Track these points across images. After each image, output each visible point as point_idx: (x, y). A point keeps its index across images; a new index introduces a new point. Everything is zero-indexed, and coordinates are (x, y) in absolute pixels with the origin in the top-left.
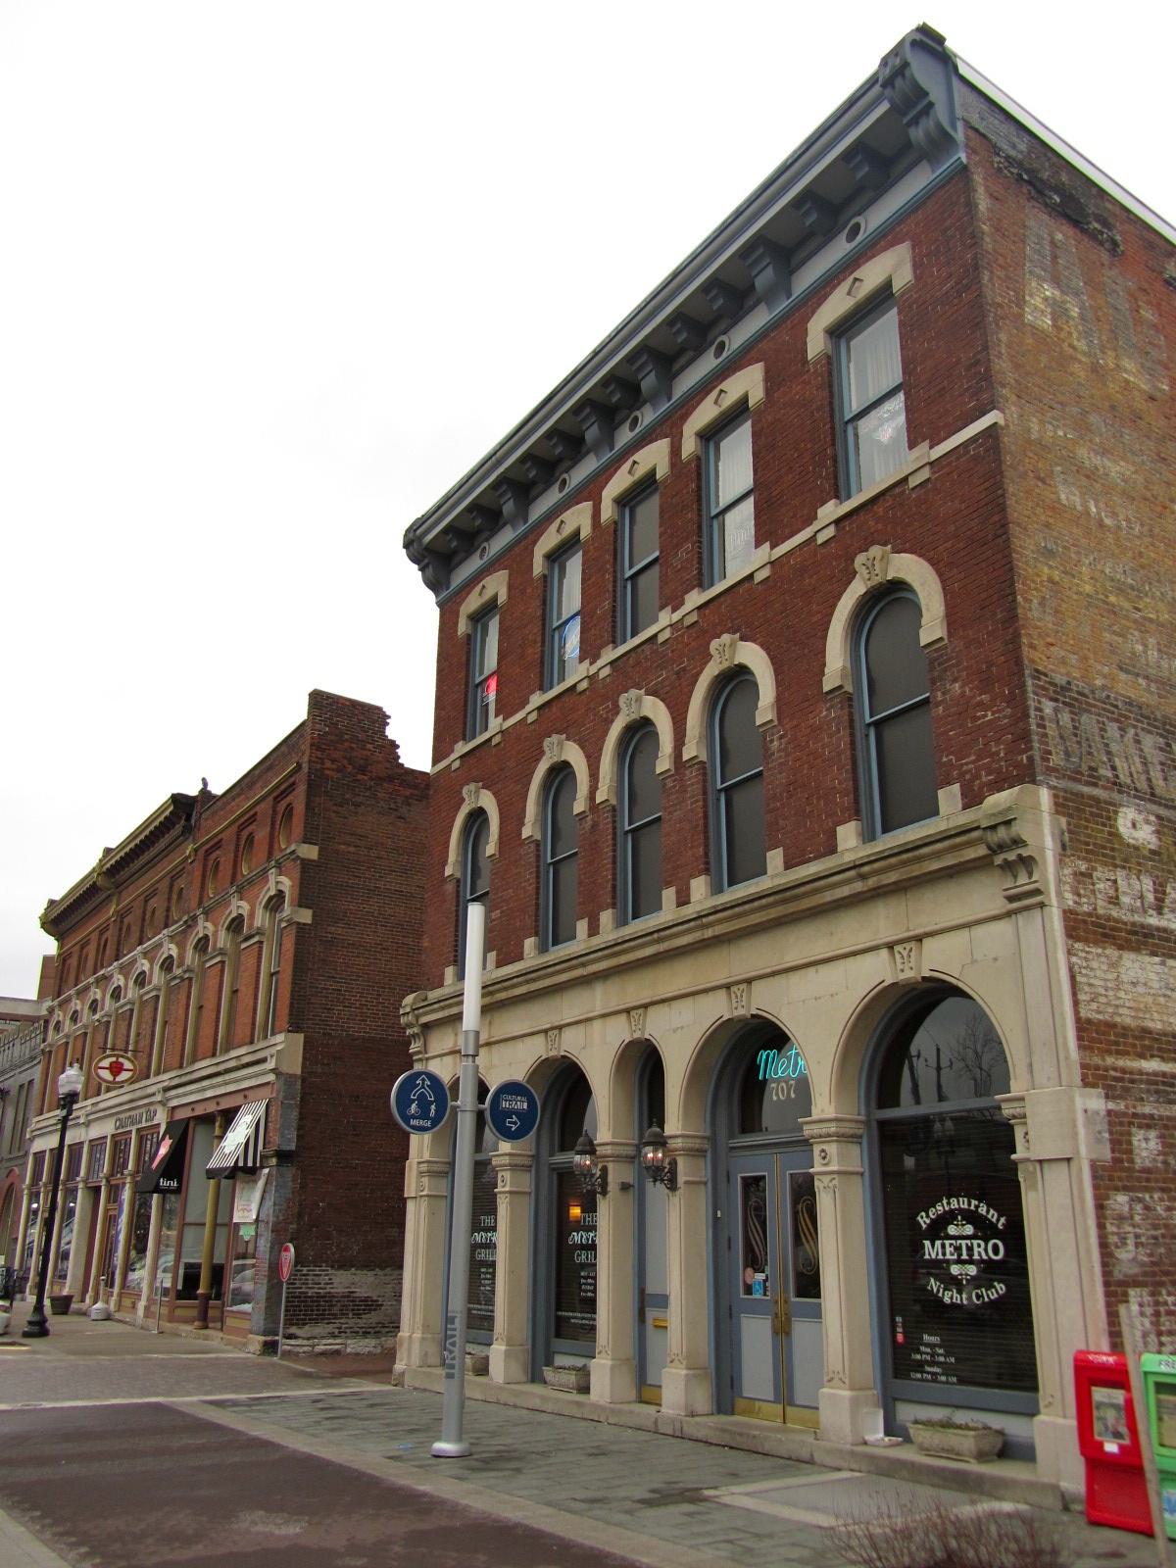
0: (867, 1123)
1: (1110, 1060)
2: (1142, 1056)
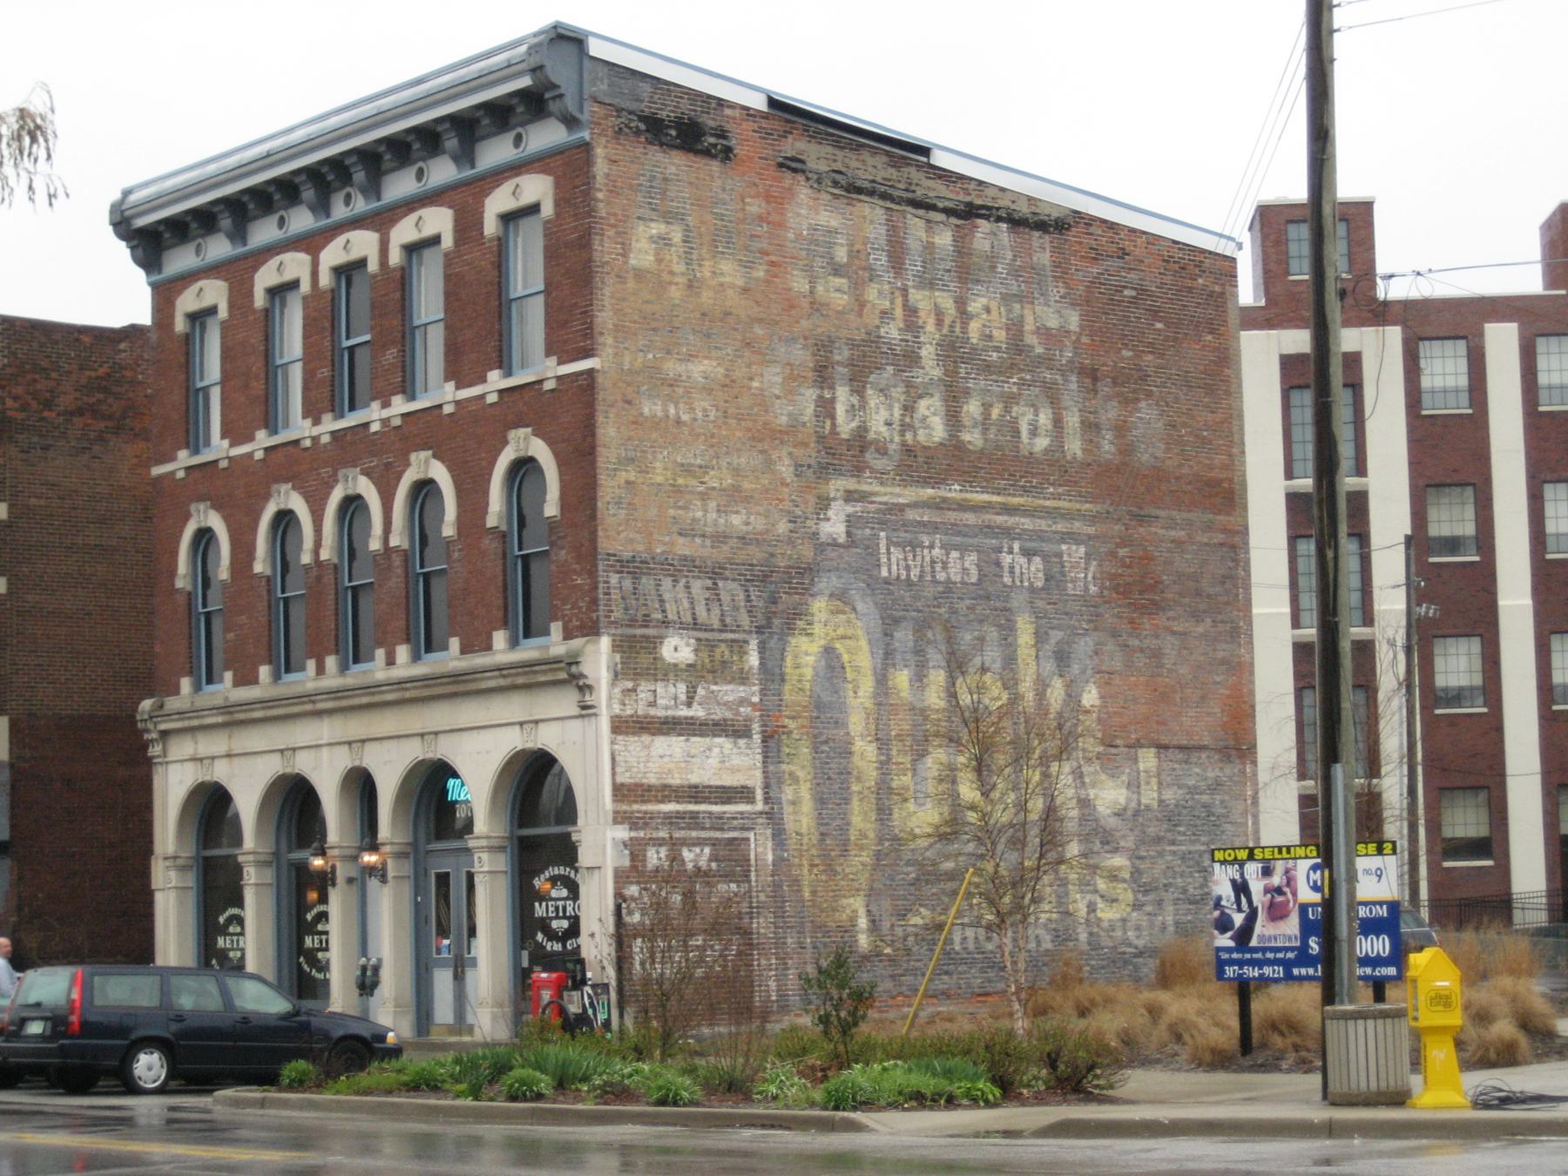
0: (511, 838)
1: (635, 807)
2: (662, 802)
